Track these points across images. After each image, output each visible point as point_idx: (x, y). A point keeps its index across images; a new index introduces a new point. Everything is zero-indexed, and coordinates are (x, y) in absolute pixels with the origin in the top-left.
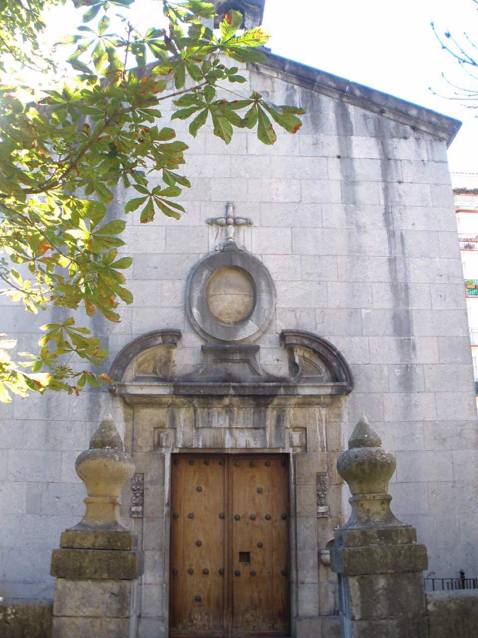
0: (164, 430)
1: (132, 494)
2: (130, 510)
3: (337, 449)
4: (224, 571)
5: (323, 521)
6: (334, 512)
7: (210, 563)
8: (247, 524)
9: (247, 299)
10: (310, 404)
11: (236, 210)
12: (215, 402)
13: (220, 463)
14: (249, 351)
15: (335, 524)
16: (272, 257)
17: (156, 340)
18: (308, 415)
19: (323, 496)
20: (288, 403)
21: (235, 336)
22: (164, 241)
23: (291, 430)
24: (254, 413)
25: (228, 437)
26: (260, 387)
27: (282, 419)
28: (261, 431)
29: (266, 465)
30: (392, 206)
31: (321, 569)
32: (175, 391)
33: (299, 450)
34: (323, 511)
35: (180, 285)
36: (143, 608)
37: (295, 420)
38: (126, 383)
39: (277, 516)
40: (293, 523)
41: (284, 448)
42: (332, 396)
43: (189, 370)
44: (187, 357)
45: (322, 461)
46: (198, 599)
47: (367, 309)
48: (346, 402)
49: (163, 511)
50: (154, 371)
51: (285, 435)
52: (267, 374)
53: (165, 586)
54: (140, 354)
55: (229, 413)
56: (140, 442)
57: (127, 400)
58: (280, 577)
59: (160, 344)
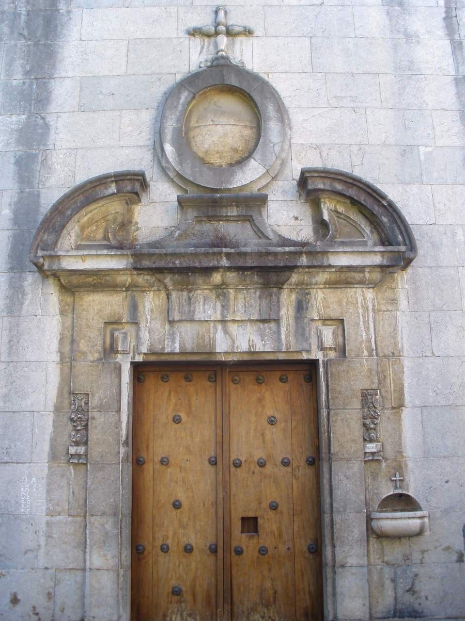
0: (120, 327)
1: (70, 427)
2: (68, 453)
3: (393, 353)
4: (216, 547)
5: (374, 465)
6: (389, 452)
7: (196, 534)
8: (253, 473)
9: (247, 132)
10: (348, 283)
11: (230, 16)
12: (199, 280)
13: (209, 379)
14: (252, 203)
15: (393, 471)
16: (283, 75)
17: (106, 188)
18: (345, 300)
19: (372, 426)
20: (314, 281)
21: (229, 181)
22: (125, 59)
23: (320, 323)
24: (260, 297)
25: (220, 335)
26: (268, 254)
27: (305, 306)
28: (273, 325)
29: (281, 380)
30: (456, 8)
31: (371, 543)
32: (135, 262)
33: (332, 355)
34: (374, 450)
35: (147, 117)
36: (87, 608)
37: (326, 307)
38: (60, 253)
39: (300, 459)
40: (325, 469)
41: (308, 351)
42: (381, 267)
43: (159, 234)
44: (156, 216)
45: (370, 370)
46: (177, 592)
47: (426, 147)
48: (403, 280)
49: (119, 453)
50: (105, 236)
51: (310, 330)
52: (280, 236)
53: (122, 572)
54: (84, 212)
55: (221, 298)
56: (83, 346)
57: (62, 281)
58: (307, 555)
59: (113, 194)
